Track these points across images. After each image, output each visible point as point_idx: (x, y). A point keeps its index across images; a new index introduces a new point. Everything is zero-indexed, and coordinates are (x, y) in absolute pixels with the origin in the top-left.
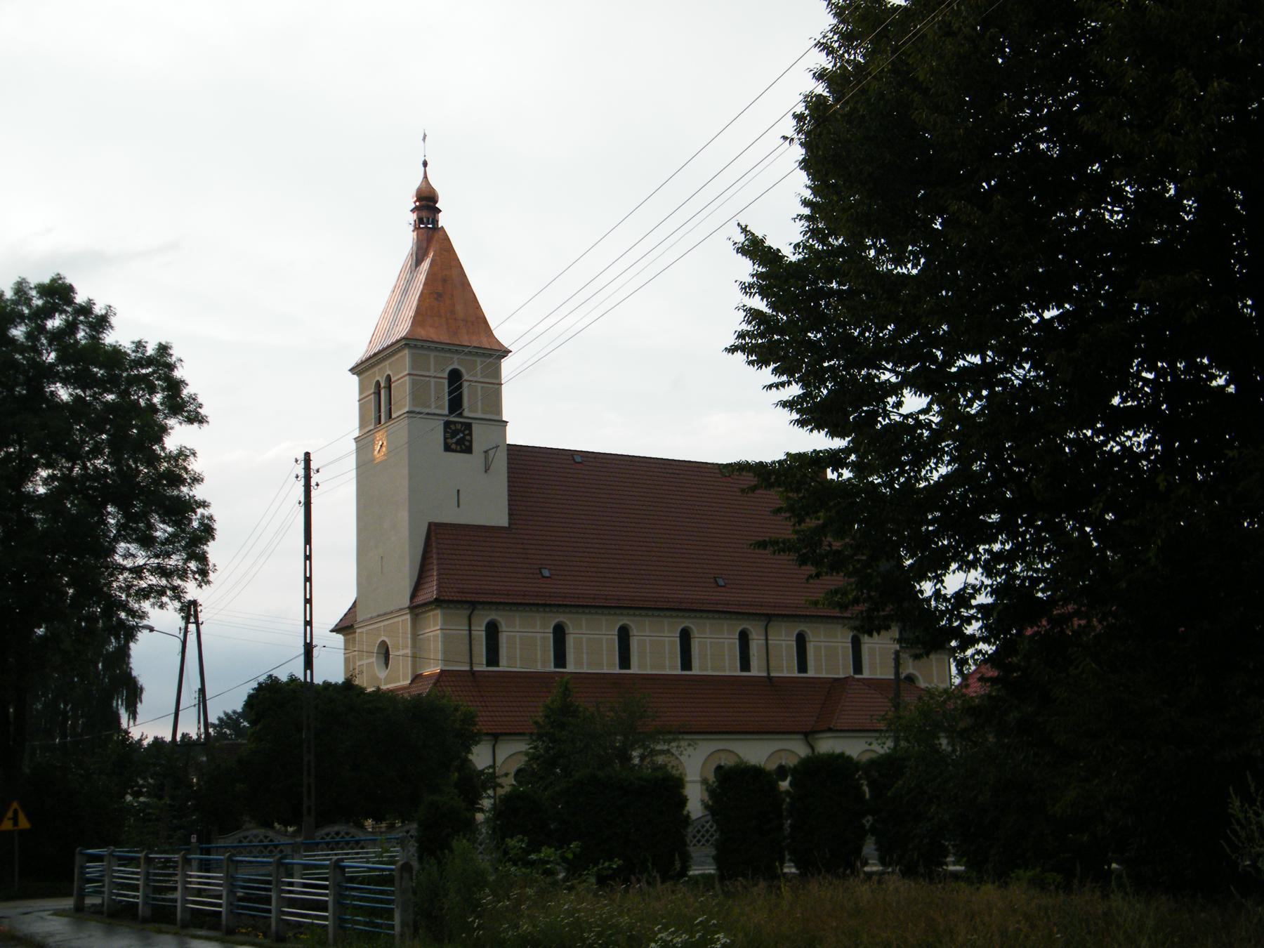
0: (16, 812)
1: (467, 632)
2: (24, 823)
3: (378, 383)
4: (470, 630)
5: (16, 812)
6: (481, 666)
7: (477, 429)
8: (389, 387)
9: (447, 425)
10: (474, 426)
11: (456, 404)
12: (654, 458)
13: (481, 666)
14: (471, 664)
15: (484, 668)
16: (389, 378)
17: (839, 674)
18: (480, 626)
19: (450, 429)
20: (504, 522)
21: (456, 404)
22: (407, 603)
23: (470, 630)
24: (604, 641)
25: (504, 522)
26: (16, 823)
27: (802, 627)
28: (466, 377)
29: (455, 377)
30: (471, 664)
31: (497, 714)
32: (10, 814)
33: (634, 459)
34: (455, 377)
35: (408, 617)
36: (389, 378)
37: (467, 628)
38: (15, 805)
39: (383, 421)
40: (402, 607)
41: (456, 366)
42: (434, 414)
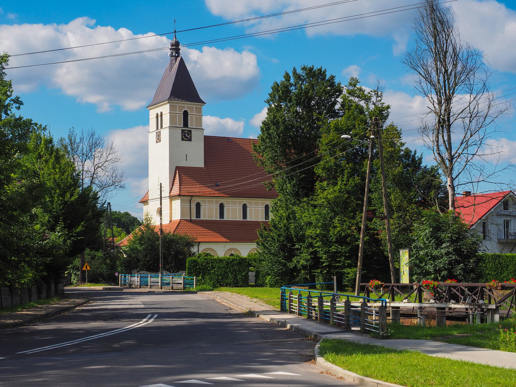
0: (86, 265)
1: (189, 206)
2: (89, 268)
3: (157, 114)
4: (190, 205)
5: (86, 265)
6: (194, 218)
7: (193, 132)
8: (161, 116)
9: (183, 131)
10: (192, 131)
11: (186, 124)
12: (221, 137)
13: (194, 218)
14: (191, 218)
15: (195, 219)
16: (162, 113)
17: (252, 219)
18: (194, 204)
19: (184, 132)
20: (202, 166)
21: (186, 124)
22: (168, 195)
23: (190, 205)
24: (230, 209)
25: (202, 166)
26: (87, 268)
27: (245, 201)
28: (189, 113)
29: (186, 114)
30: (191, 218)
31: (232, 232)
32: (85, 266)
33: (209, 137)
34: (186, 114)
35: (169, 200)
36: (162, 113)
37: (189, 205)
38: (86, 264)
39: (159, 128)
40: (166, 196)
41: (186, 109)
42: (178, 127)
